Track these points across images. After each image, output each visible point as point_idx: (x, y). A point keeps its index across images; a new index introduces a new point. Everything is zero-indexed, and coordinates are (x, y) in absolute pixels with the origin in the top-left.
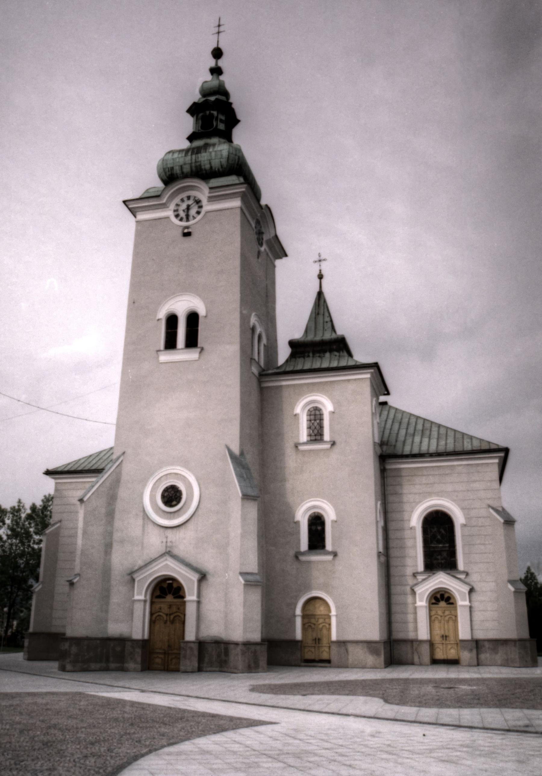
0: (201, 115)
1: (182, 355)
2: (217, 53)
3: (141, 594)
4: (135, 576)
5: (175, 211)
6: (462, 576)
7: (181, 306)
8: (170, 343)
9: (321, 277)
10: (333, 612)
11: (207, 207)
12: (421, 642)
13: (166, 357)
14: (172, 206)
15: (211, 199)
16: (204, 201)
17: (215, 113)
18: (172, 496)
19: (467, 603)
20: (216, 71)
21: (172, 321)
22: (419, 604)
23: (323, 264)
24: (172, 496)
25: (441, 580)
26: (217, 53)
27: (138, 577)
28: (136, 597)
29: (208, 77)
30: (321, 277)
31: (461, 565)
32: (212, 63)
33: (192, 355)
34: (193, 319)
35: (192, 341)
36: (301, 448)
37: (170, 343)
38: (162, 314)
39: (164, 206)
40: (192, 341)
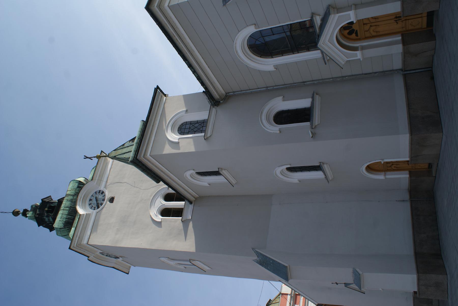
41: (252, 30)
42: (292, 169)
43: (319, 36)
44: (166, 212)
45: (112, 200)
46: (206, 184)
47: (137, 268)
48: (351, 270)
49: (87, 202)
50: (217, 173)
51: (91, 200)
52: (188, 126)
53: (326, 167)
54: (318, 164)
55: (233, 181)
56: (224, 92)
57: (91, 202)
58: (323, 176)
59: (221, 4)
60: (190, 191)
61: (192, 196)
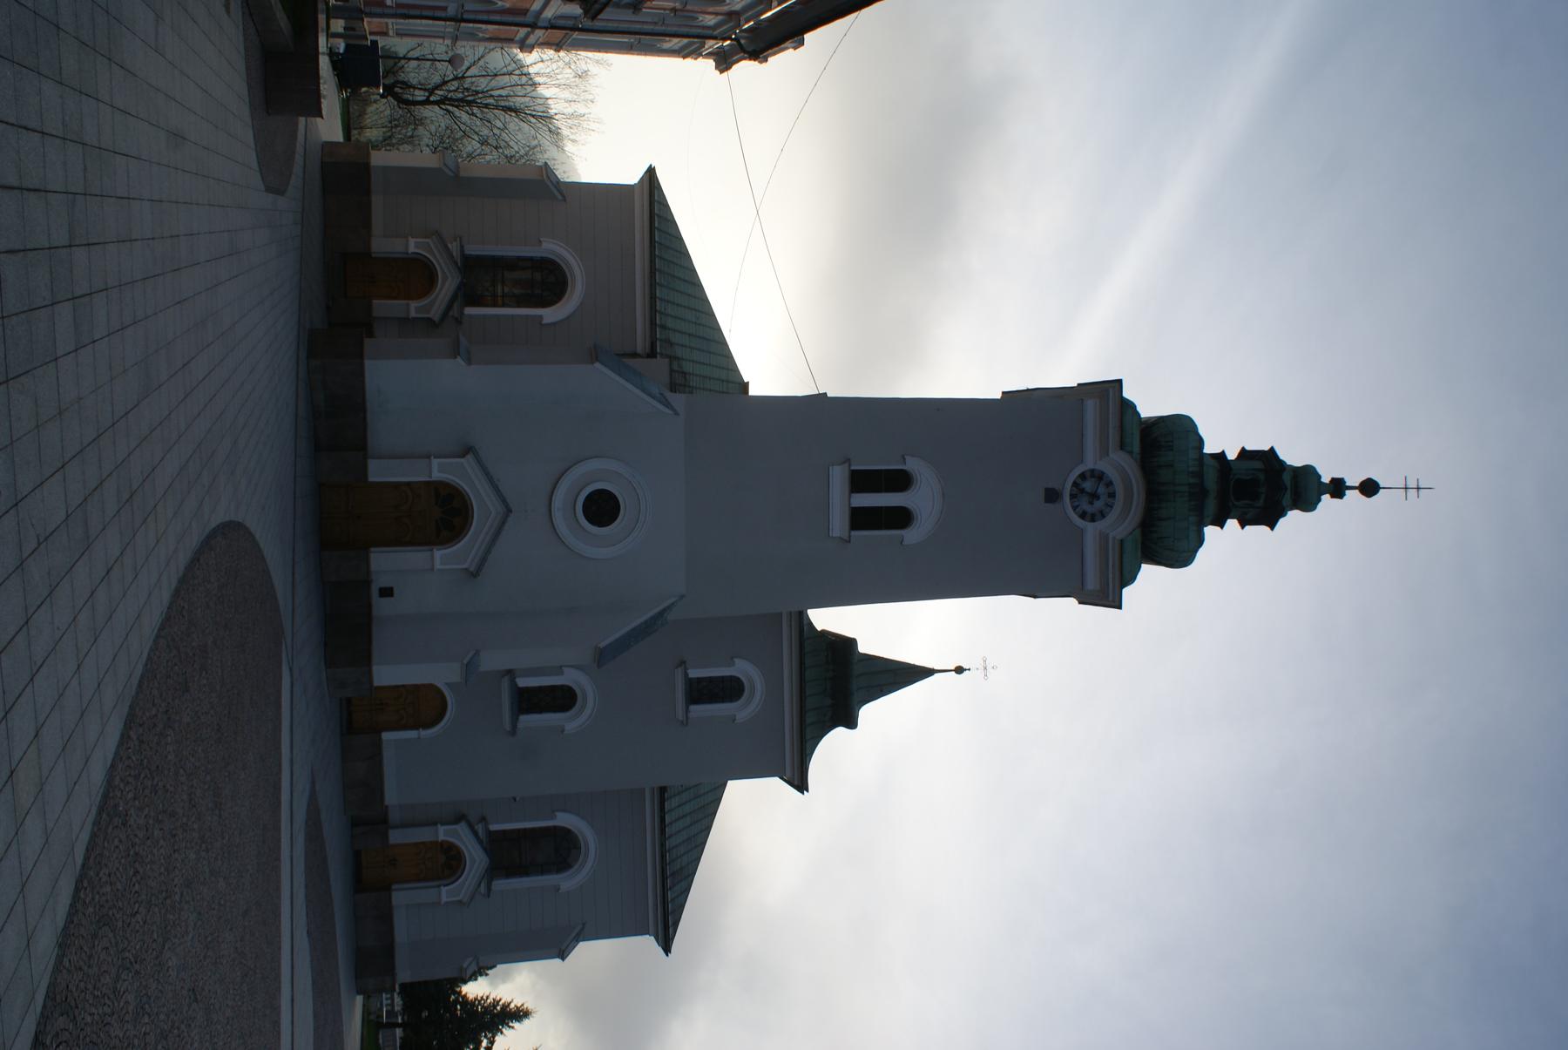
0: (1262, 477)
1: (840, 501)
2: (1369, 488)
3: (416, 246)
4: (470, 457)
5: (1092, 471)
6: (483, 889)
7: (922, 499)
8: (862, 481)
9: (959, 670)
10: (424, 733)
11: (1091, 530)
12: (386, 836)
13: (839, 478)
14: (1102, 466)
15: (1103, 538)
16: (1101, 525)
17: (1261, 503)
18: (601, 508)
19: (444, 899)
20: (1338, 488)
21: (900, 480)
22: (442, 829)
23: (981, 673)
24: (601, 508)
25: (475, 857)
26: (1369, 488)
27: (468, 462)
28: (412, 241)
29: (1326, 479)
30: (959, 670)
31: (500, 885)
32: (1353, 480)
33: (839, 522)
34: (900, 518)
35: (862, 519)
36: (680, 671)
37: (862, 481)
38: (912, 465)
39: (1104, 452)
40: (862, 519)
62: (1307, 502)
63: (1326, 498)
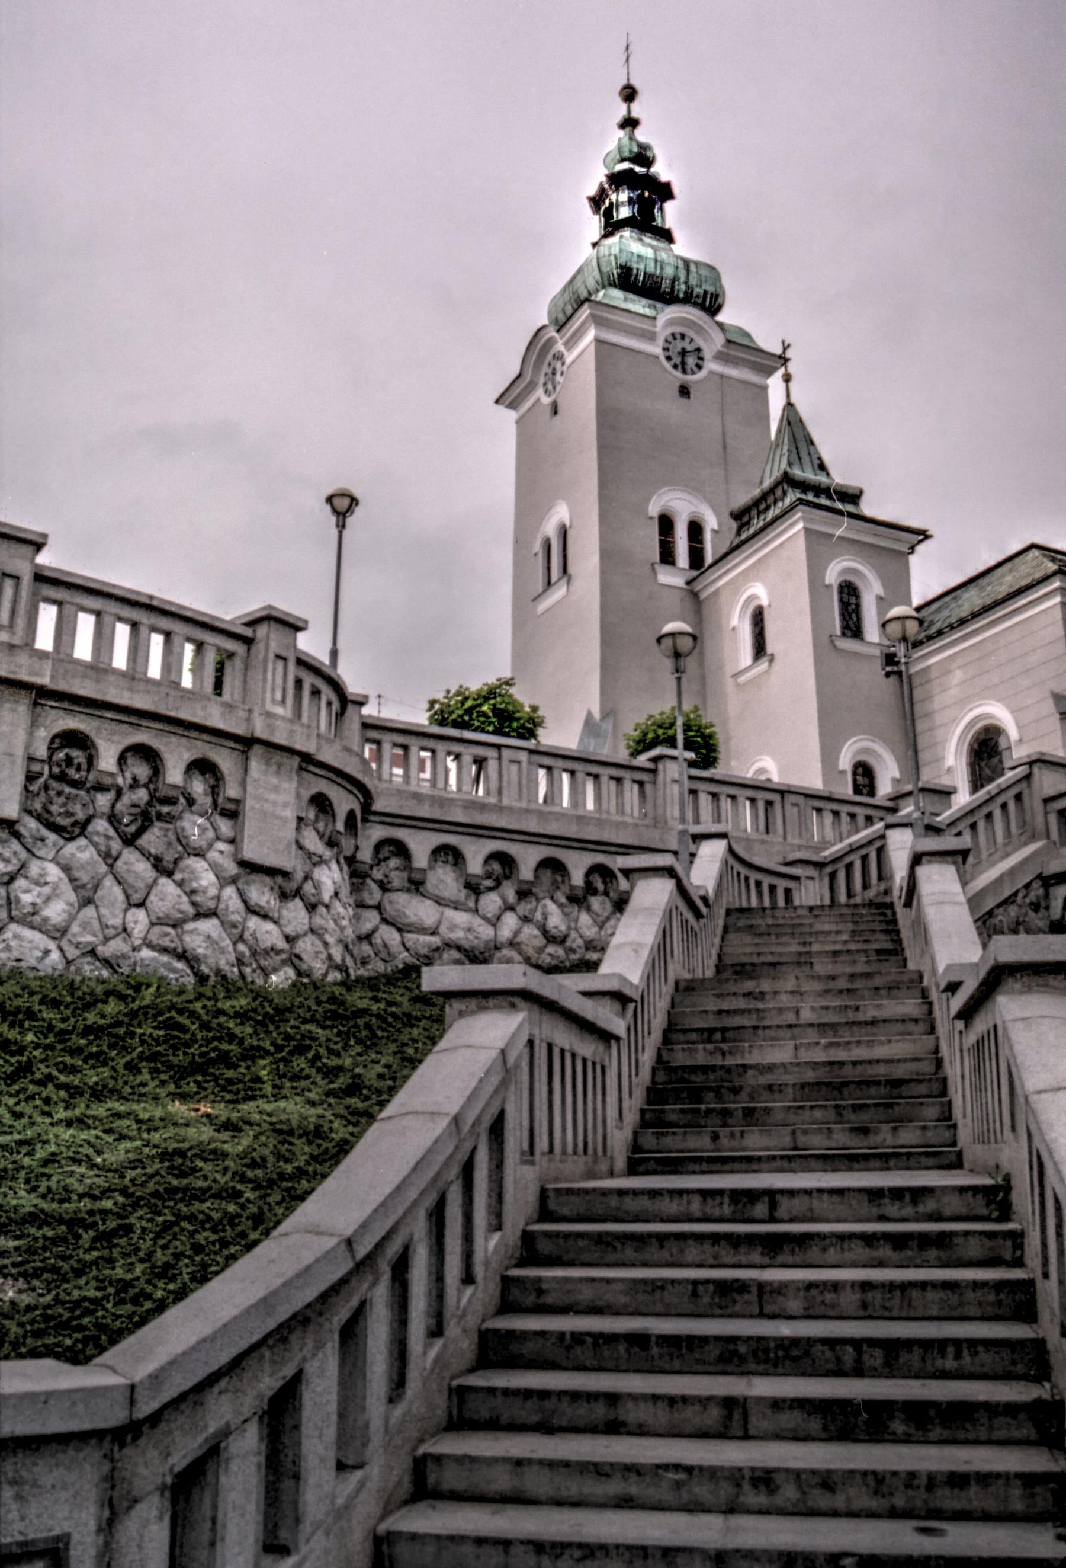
2: (629, 94)
11: (711, 366)
41: (1013, 733)
42: (758, 618)
43: (861, 1556)
44: (666, 523)
45: (684, 391)
46: (734, 621)
47: (513, 429)
48: (507, 674)
49: (678, 329)
50: (760, 648)
51: (683, 336)
52: (853, 600)
53: (763, 665)
54: (770, 648)
55: (742, 679)
56: (912, 671)
57: (678, 337)
58: (743, 666)
59: (1058, 690)
60: (721, 583)
61: (705, 587)
62: (643, 157)
63: (642, 135)
